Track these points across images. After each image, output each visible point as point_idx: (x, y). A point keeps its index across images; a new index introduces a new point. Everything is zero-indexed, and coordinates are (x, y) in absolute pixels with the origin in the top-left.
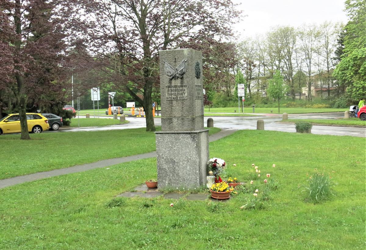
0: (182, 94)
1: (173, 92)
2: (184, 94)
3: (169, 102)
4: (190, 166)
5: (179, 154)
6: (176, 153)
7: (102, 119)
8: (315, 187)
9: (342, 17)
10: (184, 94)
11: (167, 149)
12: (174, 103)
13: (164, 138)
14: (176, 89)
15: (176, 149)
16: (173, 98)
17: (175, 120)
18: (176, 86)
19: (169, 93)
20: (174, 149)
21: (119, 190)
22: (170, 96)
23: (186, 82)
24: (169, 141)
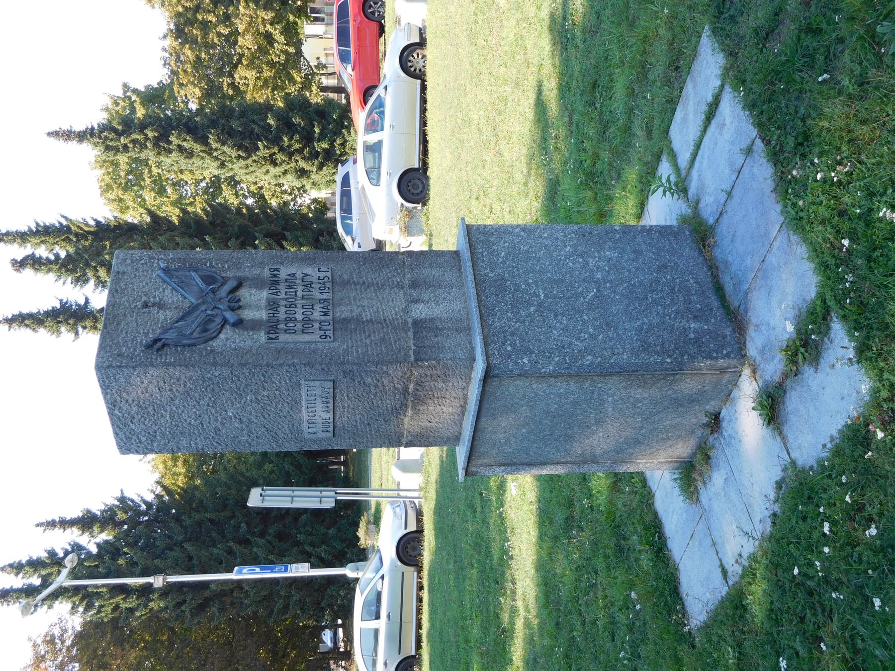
0: (308, 286)
1: (299, 317)
2: (306, 279)
3: (338, 333)
4: (603, 248)
5: (562, 281)
6: (562, 292)
7: (438, 550)
8: (842, 38)
9: (160, 21)
10: (307, 279)
11: (552, 321)
12: (346, 314)
13: (505, 332)
14: (283, 303)
15: (545, 290)
16: (326, 314)
17: (420, 311)
18: (273, 305)
19: (299, 326)
20: (546, 296)
21: (344, 58)
22: (317, 325)
23: (256, 271)
24: (515, 314)
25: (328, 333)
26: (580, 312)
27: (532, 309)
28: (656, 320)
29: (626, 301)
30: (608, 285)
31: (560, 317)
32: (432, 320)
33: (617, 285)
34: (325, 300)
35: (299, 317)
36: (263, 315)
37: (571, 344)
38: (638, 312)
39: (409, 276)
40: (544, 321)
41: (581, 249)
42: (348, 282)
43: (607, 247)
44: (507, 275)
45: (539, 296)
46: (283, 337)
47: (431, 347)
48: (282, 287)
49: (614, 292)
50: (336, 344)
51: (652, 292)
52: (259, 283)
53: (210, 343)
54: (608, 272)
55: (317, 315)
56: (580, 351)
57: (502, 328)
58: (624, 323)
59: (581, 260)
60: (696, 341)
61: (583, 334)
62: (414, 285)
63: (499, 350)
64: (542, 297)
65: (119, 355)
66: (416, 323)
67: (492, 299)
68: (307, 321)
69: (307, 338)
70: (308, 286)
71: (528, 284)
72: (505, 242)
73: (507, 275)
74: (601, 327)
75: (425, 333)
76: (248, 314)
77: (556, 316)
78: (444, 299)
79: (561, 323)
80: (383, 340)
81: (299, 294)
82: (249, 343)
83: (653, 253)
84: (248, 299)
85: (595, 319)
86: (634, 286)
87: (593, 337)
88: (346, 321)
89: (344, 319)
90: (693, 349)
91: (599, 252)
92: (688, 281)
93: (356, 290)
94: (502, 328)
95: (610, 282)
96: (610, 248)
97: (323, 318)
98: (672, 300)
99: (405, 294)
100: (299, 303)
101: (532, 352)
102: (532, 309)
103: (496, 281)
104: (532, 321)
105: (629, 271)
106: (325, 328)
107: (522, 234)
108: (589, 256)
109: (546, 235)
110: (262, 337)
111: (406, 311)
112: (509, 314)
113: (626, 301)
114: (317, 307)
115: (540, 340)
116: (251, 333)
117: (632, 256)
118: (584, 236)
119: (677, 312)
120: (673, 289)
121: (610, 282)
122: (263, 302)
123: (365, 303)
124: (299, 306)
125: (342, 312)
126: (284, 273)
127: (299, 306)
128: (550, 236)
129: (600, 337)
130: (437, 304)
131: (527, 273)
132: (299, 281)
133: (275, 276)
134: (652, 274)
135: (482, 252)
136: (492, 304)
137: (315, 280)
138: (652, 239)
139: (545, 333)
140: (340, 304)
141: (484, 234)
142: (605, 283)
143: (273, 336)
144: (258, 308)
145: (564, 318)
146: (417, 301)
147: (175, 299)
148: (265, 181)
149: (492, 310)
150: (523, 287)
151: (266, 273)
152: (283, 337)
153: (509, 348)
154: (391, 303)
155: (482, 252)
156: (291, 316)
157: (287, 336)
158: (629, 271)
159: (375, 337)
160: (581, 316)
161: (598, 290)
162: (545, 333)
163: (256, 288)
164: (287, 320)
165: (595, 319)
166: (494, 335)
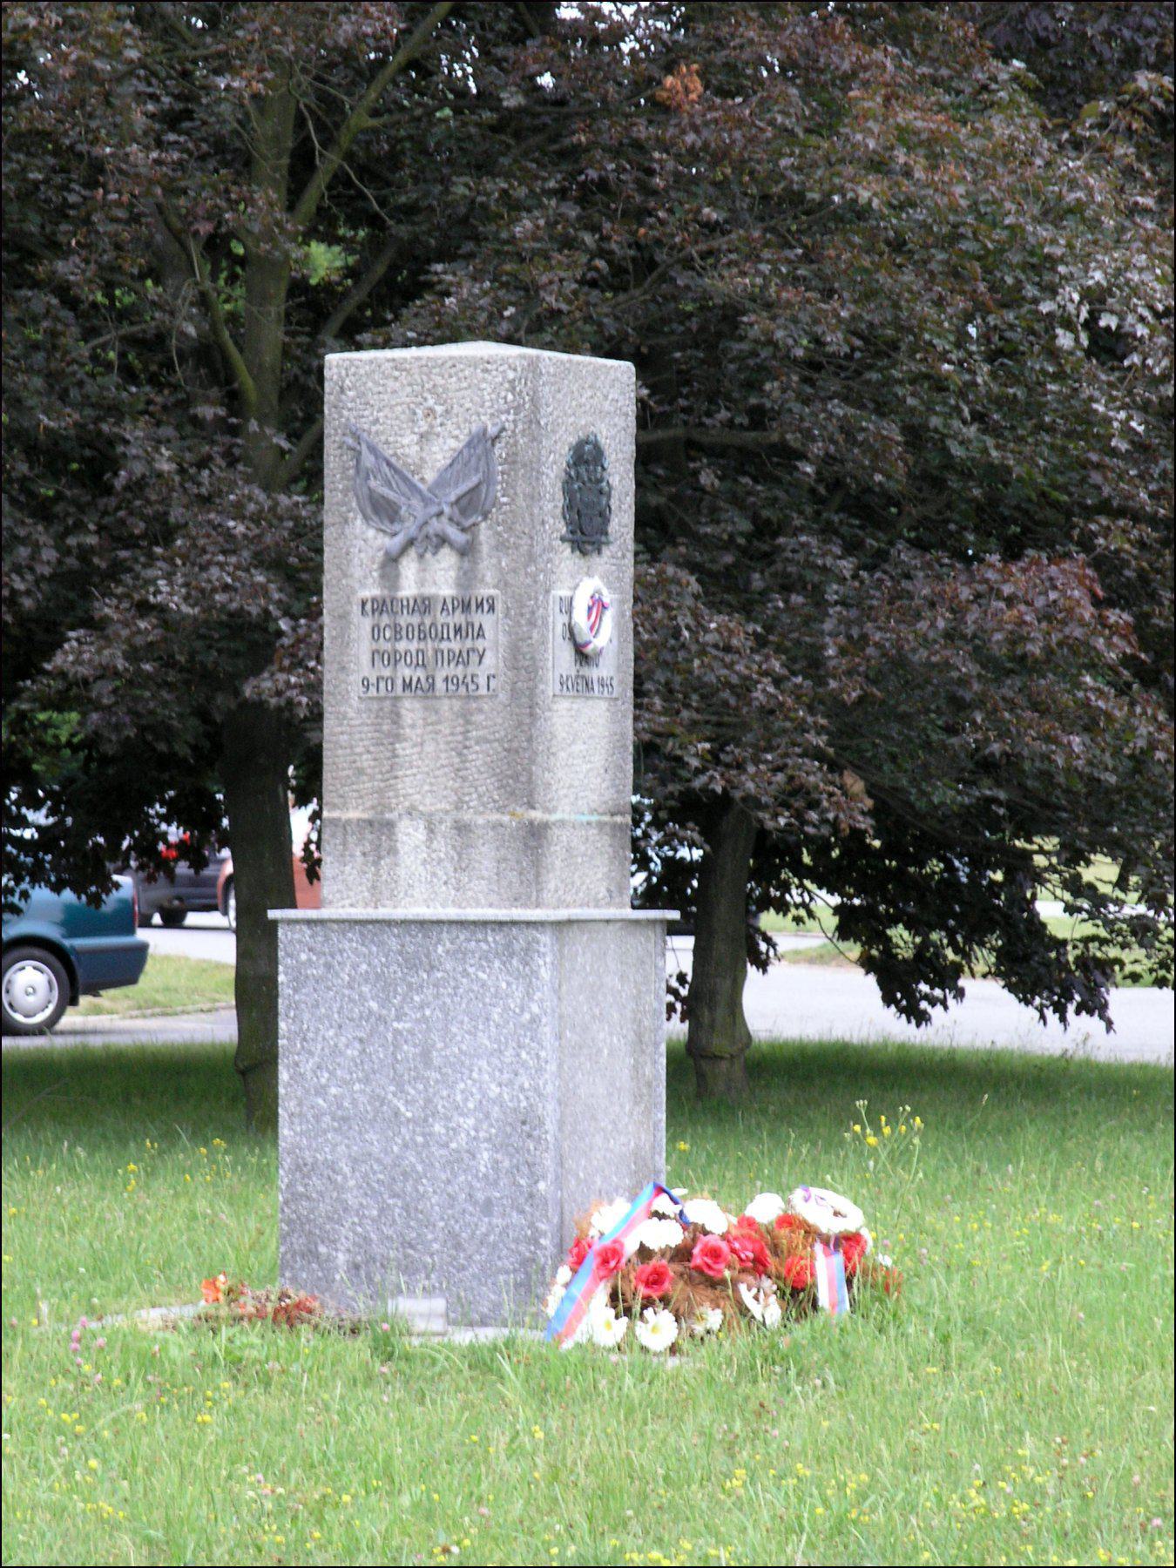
3: (375, 706)
5: (427, 1063)
10: (474, 658)
14: (428, 621)
17: (410, 835)
18: (423, 605)
19: (384, 646)
20: (397, 1032)
22: (387, 673)
23: (490, 577)
25: (373, 690)
26: (366, 1081)
27: (374, 1005)
28: (351, 1200)
29: (388, 1160)
30: (420, 1139)
31: (357, 1045)
32: (393, 851)
33: (419, 1153)
34: (432, 686)
35: (402, 646)
36: (409, 588)
37: (311, 1053)
38: (366, 1174)
39: (481, 821)
40: (351, 1020)
41: (496, 1112)
42: (468, 722)
43: (499, 1157)
44: (439, 975)
45: (398, 1019)
46: (367, 623)
47: (344, 844)
48: (459, 618)
49: (406, 1146)
50: (355, 702)
51: (406, 1208)
52: (467, 578)
53: (360, 516)
54: (446, 1145)
55: (405, 672)
56: (297, 1064)
57: (341, 952)
58: (348, 1147)
59: (471, 1105)
60: (311, 1254)
61: (326, 1075)
62: (462, 828)
63: (300, 942)
64: (395, 1025)
65: (342, 388)
66: (390, 825)
67: (394, 944)
68: (394, 659)
69: (365, 658)
70: (461, 658)
71: (422, 1007)
72: (509, 984)
73: (439, 975)
74: (340, 1107)
75: (370, 837)
76: (409, 568)
77: (361, 1041)
78: (434, 874)
79: (347, 1046)
80: (360, 771)
81: (444, 645)
82: (358, 573)
83: (486, 1235)
84: (437, 566)
85: (354, 1102)
86: (418, 1181)
87: (321, 1091)
88: (396, 718)
89: (398, 715)
90: (299, 1242)
91: (489, 1140)
92: (428, 1277)
93: (452, 734)
94: (341, 952)
95: (426, 1145)
96: (497, 1162)
97: (399, 682)
98: (389, 1238)
99: (447, 812)
100: (430, 646)
101: (296, 990)
102: (374, 1005)
103: (427, 956)
104: (351, 1000)
105: (449, 1182)
106: (382, 685)
107: (527, 1016)
108: (478, 1121)
109: (524, 1055)
110: (372, 591)
111: (410, 812)
112: (364, 967)
113: (388, 1160)
114: (420, 673)
115: (317, 1006)
116: (375, 574)
117: (480, 1196)
118: (524, 1123)
119: (367, 1240)
120: (411, 1246)
121: (426, 1145)
122: (429, 590)
123: (429, 748)
124: (422, 645)
125: (412, 711)
126: (486, 620)
127: (422, 645)
128: (524, 1064)
129: (321, 1101)
130: (424, 862)
131: (444, 1009)
132: (469, 643)
133: (480, 605)
134: (442, 1219)
135: (486, 942)
136: (383, 943)
137: (470, 670)
138: (517, 1241)
139: (328, 1017)
140: (426, 709)
141: (527, 951)
142: (424, 1135)
143: (368, 607)
144: (421, 583)
145: (356, 1053)
146: (431, 830)
147: (439, 457)
148: (404, 633)
149: (372, 941)
150: (416, 998)
151: (485, 592)
152: (367, 623)
153: (303, 957)
154: (427, 788)
155: (486, 942)
156: (404, 633)
157: (369, 629)
158: (449, 1182)
159: (366, 761)
160: (359, 1081)
161: (408, 1120)
162: (328, 1017)
163: (458, 578)
164: (396, 630)
165: (354, 1102)
166: (327, 939)
